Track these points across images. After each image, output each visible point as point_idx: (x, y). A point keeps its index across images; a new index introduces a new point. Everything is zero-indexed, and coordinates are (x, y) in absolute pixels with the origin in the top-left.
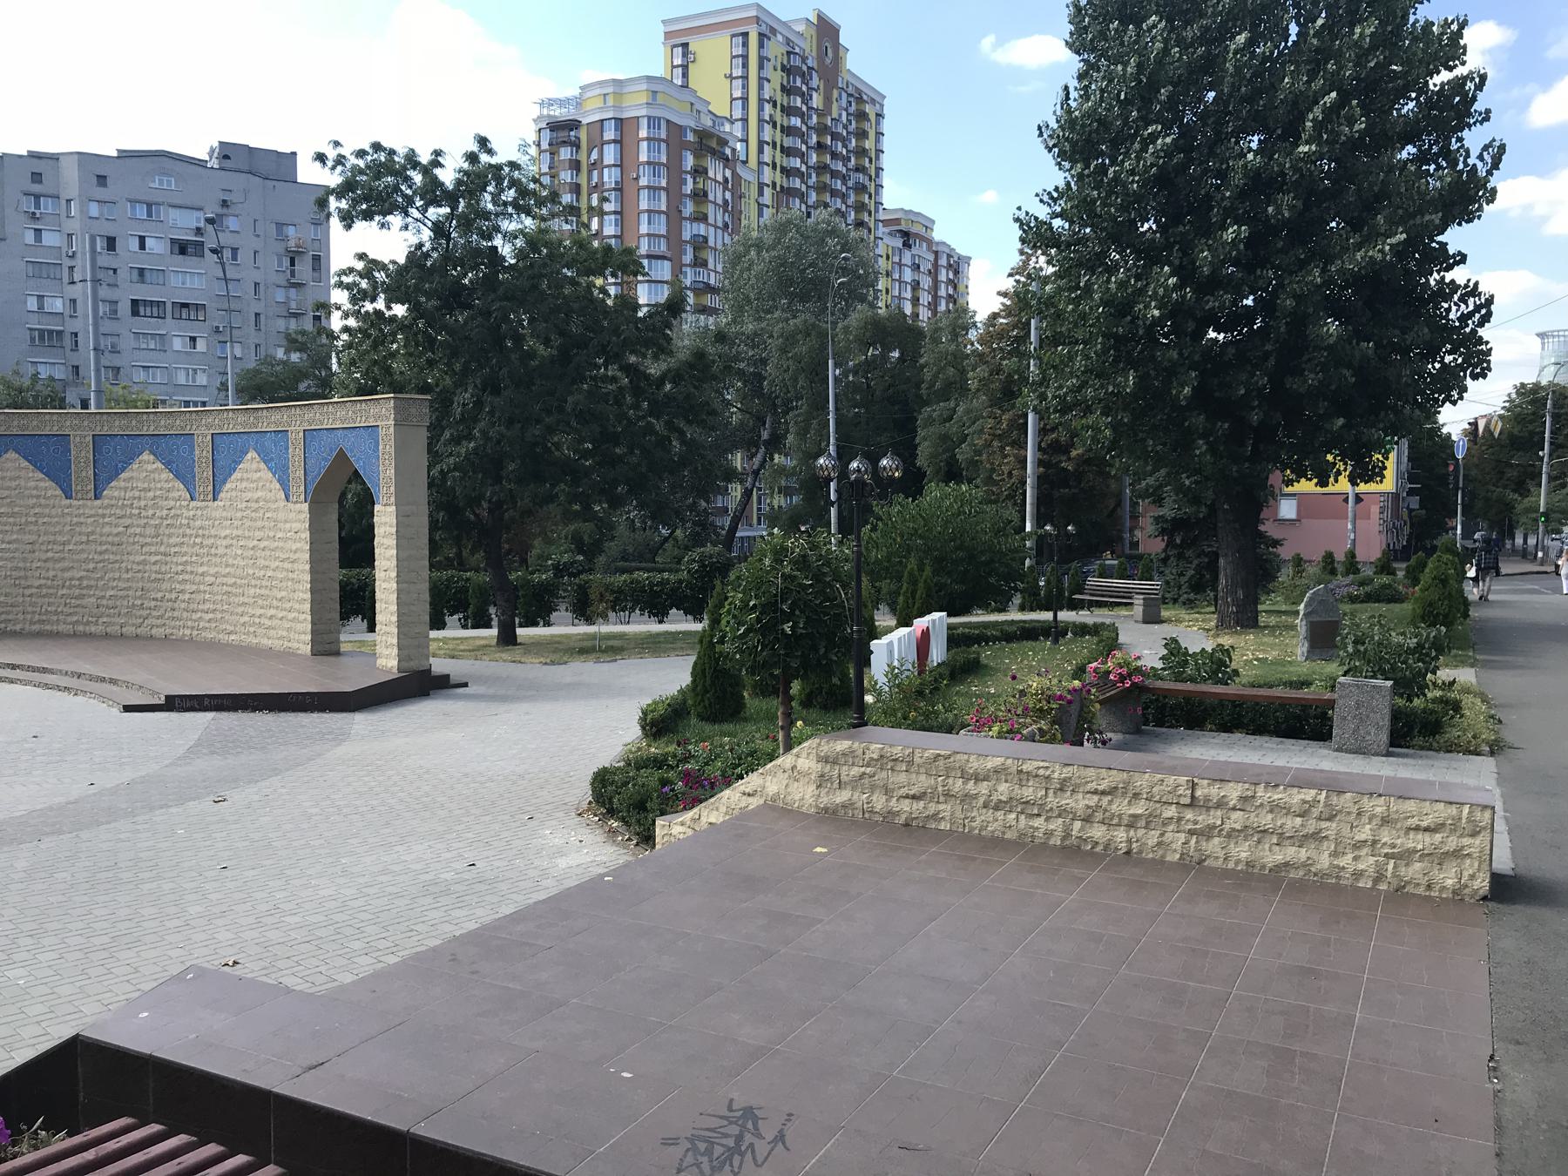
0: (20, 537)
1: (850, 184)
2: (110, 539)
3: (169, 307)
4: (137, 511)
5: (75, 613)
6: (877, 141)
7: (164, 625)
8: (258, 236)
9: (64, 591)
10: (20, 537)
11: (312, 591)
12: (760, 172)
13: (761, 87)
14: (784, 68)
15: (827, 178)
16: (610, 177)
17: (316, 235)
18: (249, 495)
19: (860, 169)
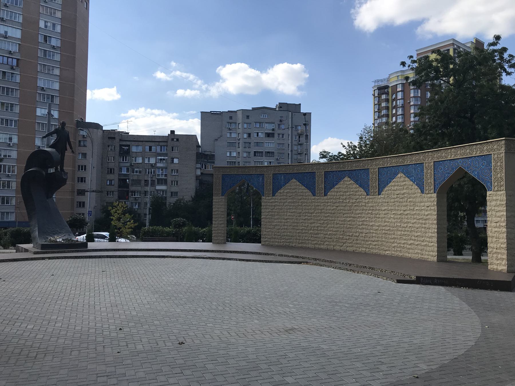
2: (330, 211)
3: (264, 153)
7: (352, 246)
9: (311, 232)
11: (438, 233)
16: (400, 103)
18: (398, 192)
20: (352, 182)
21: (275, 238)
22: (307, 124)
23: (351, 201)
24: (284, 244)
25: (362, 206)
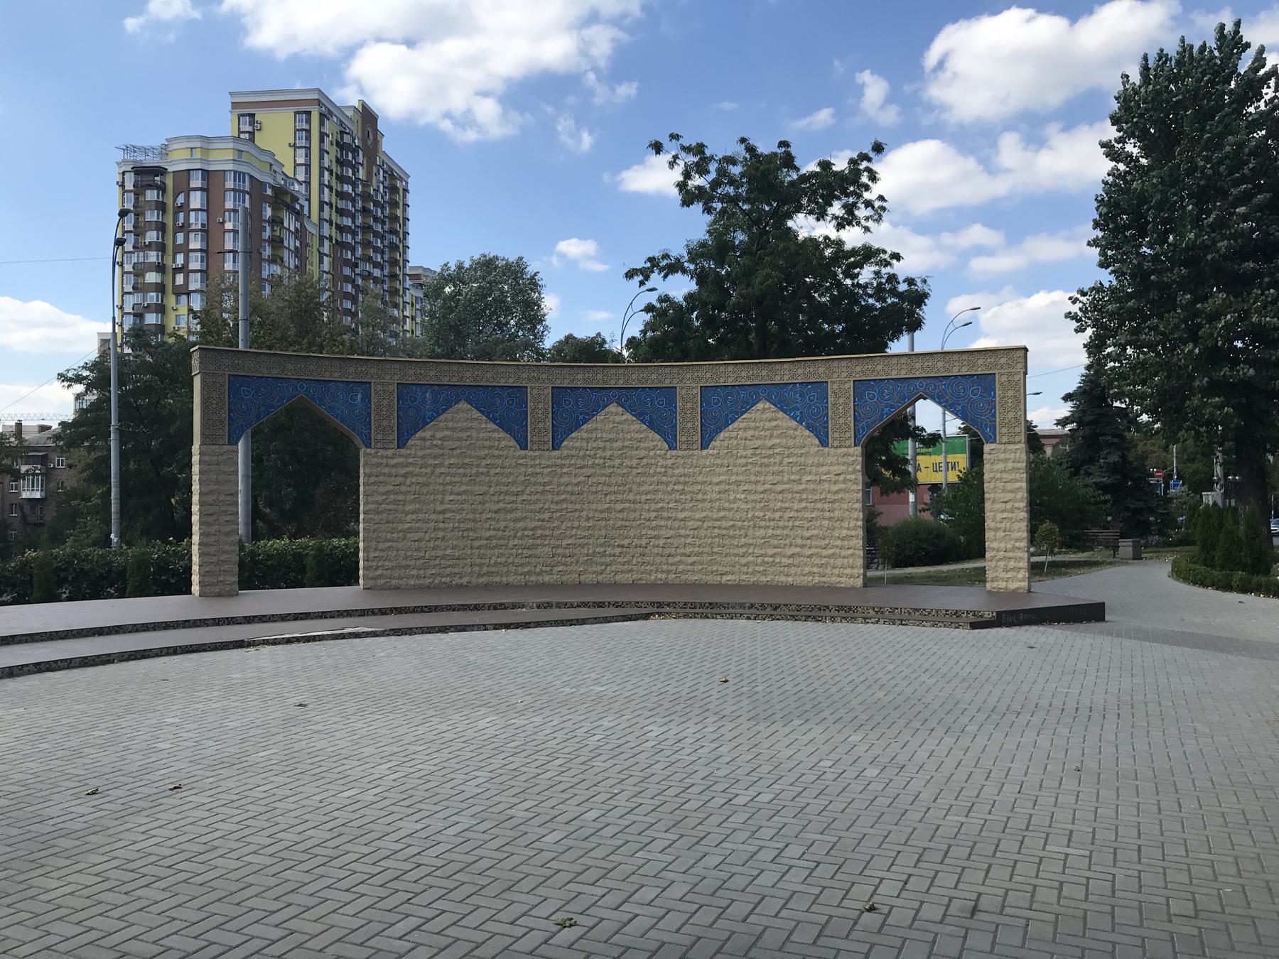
0: (469, 488)
1: (386, 243)
2: (569, 488)
5: (528, 564)
6: (404, 211)
10: (469, 488)
12: (320, 227)
13: (321, 158)
14: (338, 144)
15: (371, 237)
16: (196, 220)
19: (393, 232)
20: (630, 417)
23: (627, 462)
24: (436, 581)
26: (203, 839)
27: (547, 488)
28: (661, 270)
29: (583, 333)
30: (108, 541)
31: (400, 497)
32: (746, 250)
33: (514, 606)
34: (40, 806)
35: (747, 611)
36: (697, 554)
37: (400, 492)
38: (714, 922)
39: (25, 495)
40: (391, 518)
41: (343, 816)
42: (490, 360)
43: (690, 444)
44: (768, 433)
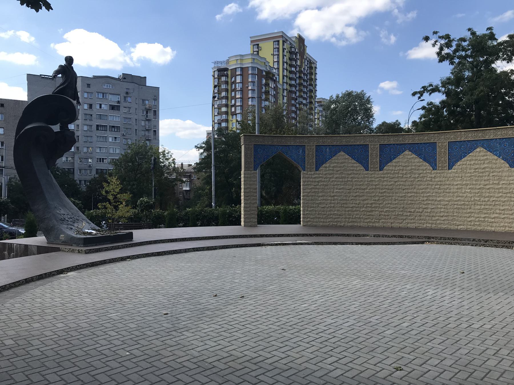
0: (344, 187)
1: (308, 89)
2: (387, 187)
4: (401, 175)
6: (315, 76)
8: (137, 104)
10: (344, 187)
12: (283, 85)
13: (283, 58)
15: (302, 88)
16: (239, 87)
17: (155, 103)
19: (311, 85)
21: (319, 218)
22: (156, 98)
23: (413, 176)
24: (331, 224)
25: (427, 181)
26: (254, 317)
27: (377, 187)
28: (428, 91)
29: (390, 120)
30: (211, 206)
31: (316, 190)
32: (470, 79)
33: (364, 236)
34: (199, 299)
35: (471, 242)
36: (446, 216)
37: (316, 188)
38: (467, 378)
39: (184, 189)
40: (313, 198)
41: (304, 314)
42: (350, 134)
43: (443, 168)
44: (482, 162)
